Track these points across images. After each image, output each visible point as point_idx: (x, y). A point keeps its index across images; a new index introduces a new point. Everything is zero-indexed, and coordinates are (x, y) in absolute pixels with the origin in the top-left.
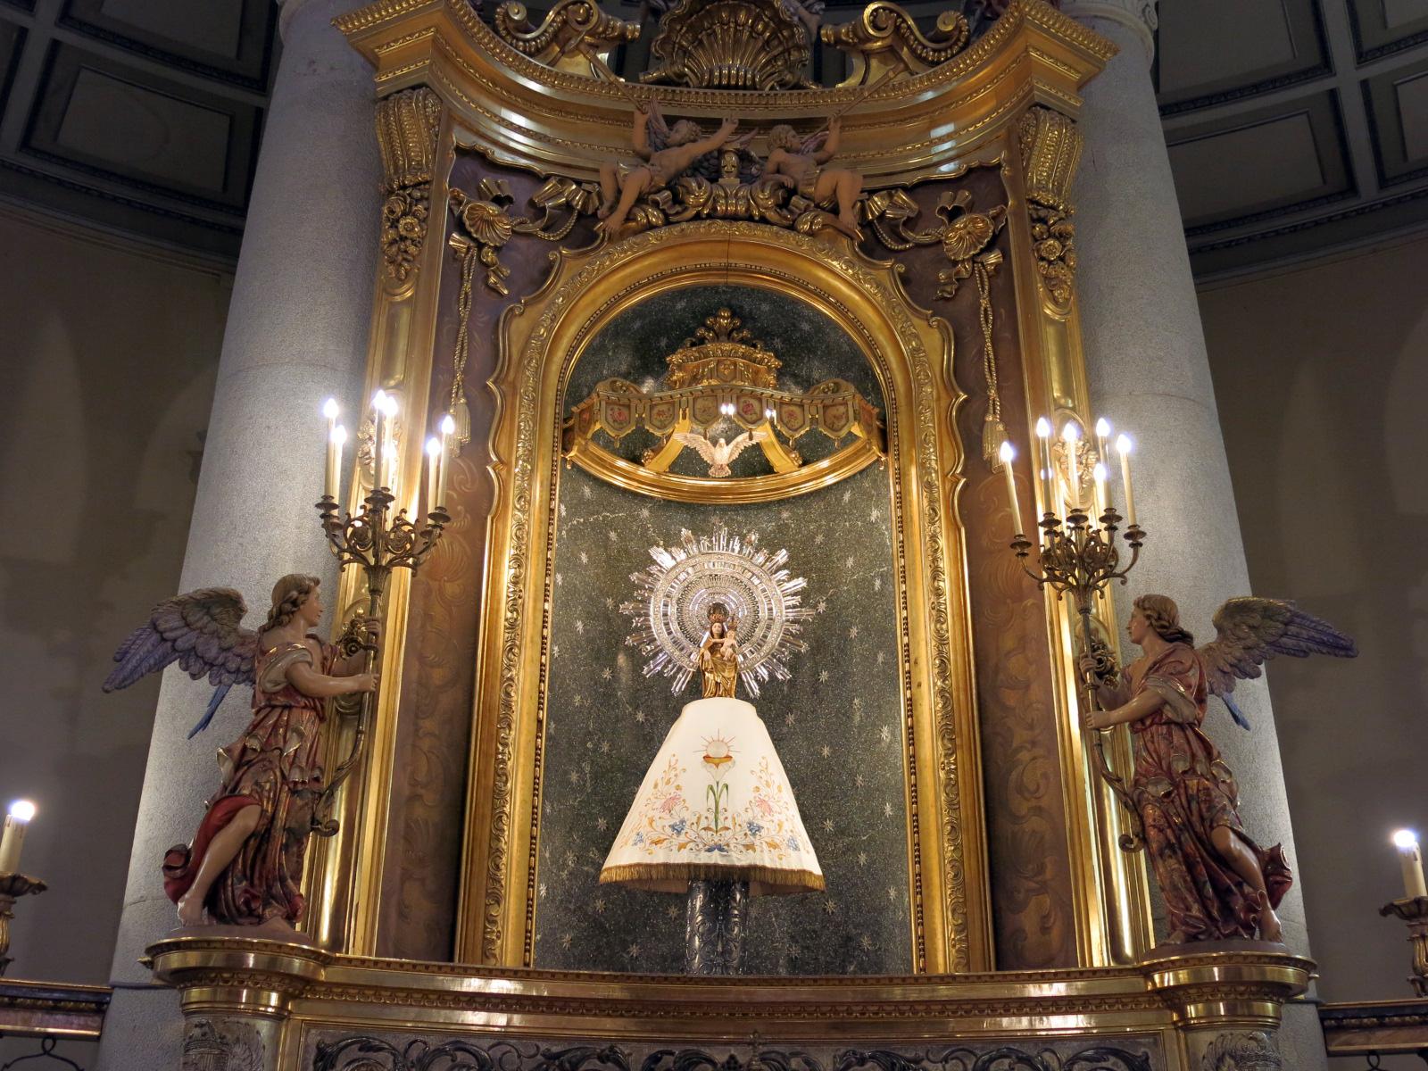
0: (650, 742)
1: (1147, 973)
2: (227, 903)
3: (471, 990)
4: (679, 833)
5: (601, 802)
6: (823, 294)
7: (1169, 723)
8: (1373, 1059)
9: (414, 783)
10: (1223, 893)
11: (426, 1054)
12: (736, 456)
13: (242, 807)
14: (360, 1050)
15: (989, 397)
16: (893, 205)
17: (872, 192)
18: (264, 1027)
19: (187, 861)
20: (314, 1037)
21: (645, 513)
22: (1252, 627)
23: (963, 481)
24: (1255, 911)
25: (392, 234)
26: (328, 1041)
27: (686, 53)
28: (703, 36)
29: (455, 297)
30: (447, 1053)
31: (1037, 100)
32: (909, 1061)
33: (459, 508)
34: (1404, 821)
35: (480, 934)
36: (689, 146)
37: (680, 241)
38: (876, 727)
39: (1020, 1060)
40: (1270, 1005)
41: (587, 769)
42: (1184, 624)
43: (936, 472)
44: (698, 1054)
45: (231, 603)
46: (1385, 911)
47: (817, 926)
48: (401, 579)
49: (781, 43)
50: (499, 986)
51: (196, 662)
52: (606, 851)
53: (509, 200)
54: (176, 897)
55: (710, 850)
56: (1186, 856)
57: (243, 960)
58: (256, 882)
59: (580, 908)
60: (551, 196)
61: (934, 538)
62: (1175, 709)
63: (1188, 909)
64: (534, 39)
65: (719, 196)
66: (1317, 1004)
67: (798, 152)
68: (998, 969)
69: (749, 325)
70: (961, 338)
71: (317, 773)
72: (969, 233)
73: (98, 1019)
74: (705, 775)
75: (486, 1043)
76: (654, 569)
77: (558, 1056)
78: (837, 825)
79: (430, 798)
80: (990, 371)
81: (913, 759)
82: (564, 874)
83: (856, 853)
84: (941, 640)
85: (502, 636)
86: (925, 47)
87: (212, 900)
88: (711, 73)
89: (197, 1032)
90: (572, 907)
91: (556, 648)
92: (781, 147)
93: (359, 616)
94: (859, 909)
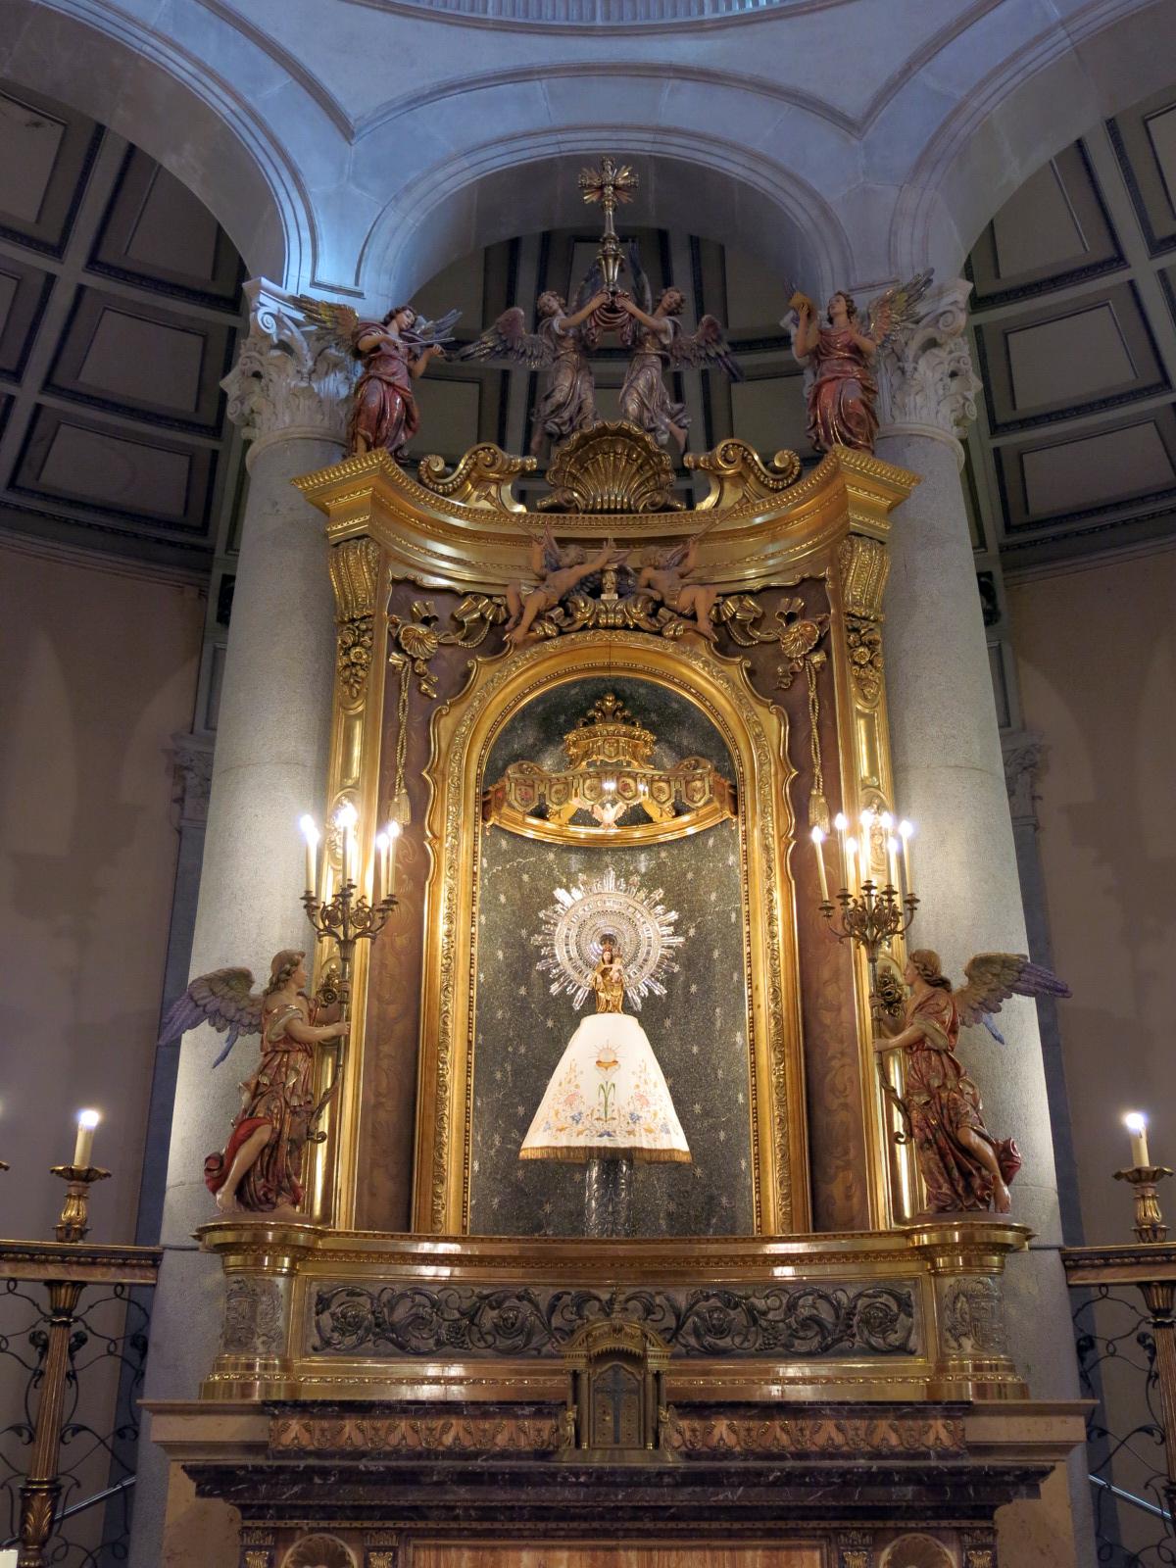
0: (557, 1044)
1: (907, 1235)
2: (251, 1196)
3: (424, 1251)
4: (577, 1122)
5: (520, 1094)
6: (686, 685)
7: (929, 1049)
8: (1104, 1290)
9: (378, 1094)
10: (966, 1175)
11: (393, 1297)
12: (620, 814)
13: (258, 1126)
14: (348, 1295)
15: (814, 775)
16: (742, 609)
17: (726, 596)
18: (281, 1281)
19: (222, 1164)
20: (315, 1287)
21: (551, 856)
22: (994, 975)
23: (794, 842)
24: (989, 1189)
25: (345, 661)
26: (325, 1290)
27: (575, 478)
28: (588, 465)
29: (395, 706)
30: (408, 1296)
31: (852, 530)
32: (740, 1297)
33: (404, 876)
34: (1136, 1105)
35: (429, 1206)
36: (577, 568)
37: (571, 647)
38: (732, 1032)
39: (821, 1297)
40: (996, 1258)
41: (509, 1068)
42: (945, 973)
43: (773, 837)
44: (589, 1293)
45: (244, 977)
46: (1118, 1176)
47: (689, 1188)
48: (362, 946)
49: (651, 468)
50: (442, 1248)
51: (219, 1019)
52: (524, 1132)
53: (435, 618)
54: (215, 1189)
55: (601, 1136)
56: (939, 1148)
57: (265, 1236)
58: (270, 1178)
59: (505, 1177)
60: (469, 612)
61: (770, 891)
62: (932, 1040)
63: (940, 1188)
64: (451, 482)
65: (601, 610)
66: (1060, 1249)
67: (664, 568)
68: (815, 1230)
69: (631, 703)
70: (795, 723)
71: (309, 1098)
72: (801, 635)
73: (153, 1271)
74: (596, 1077)
75: (436, 1288)
76: (558, 907)
77: (487, 1297)
78: (703, 1109)
79: (390, 1104)
80: (816, 753)
81: (754, 1063)
82: (492, 1152)
83: (717, 1131)
84: (775, 974)
85: (439, 978)
86: (766, 476)
87: (240, 1191)
88: (595, 499)
89: (235, 1286)
90: (499, 1177)
91: (482, 976)
92: (650, 566)
93: (333, 970)
94: (719, 1176)
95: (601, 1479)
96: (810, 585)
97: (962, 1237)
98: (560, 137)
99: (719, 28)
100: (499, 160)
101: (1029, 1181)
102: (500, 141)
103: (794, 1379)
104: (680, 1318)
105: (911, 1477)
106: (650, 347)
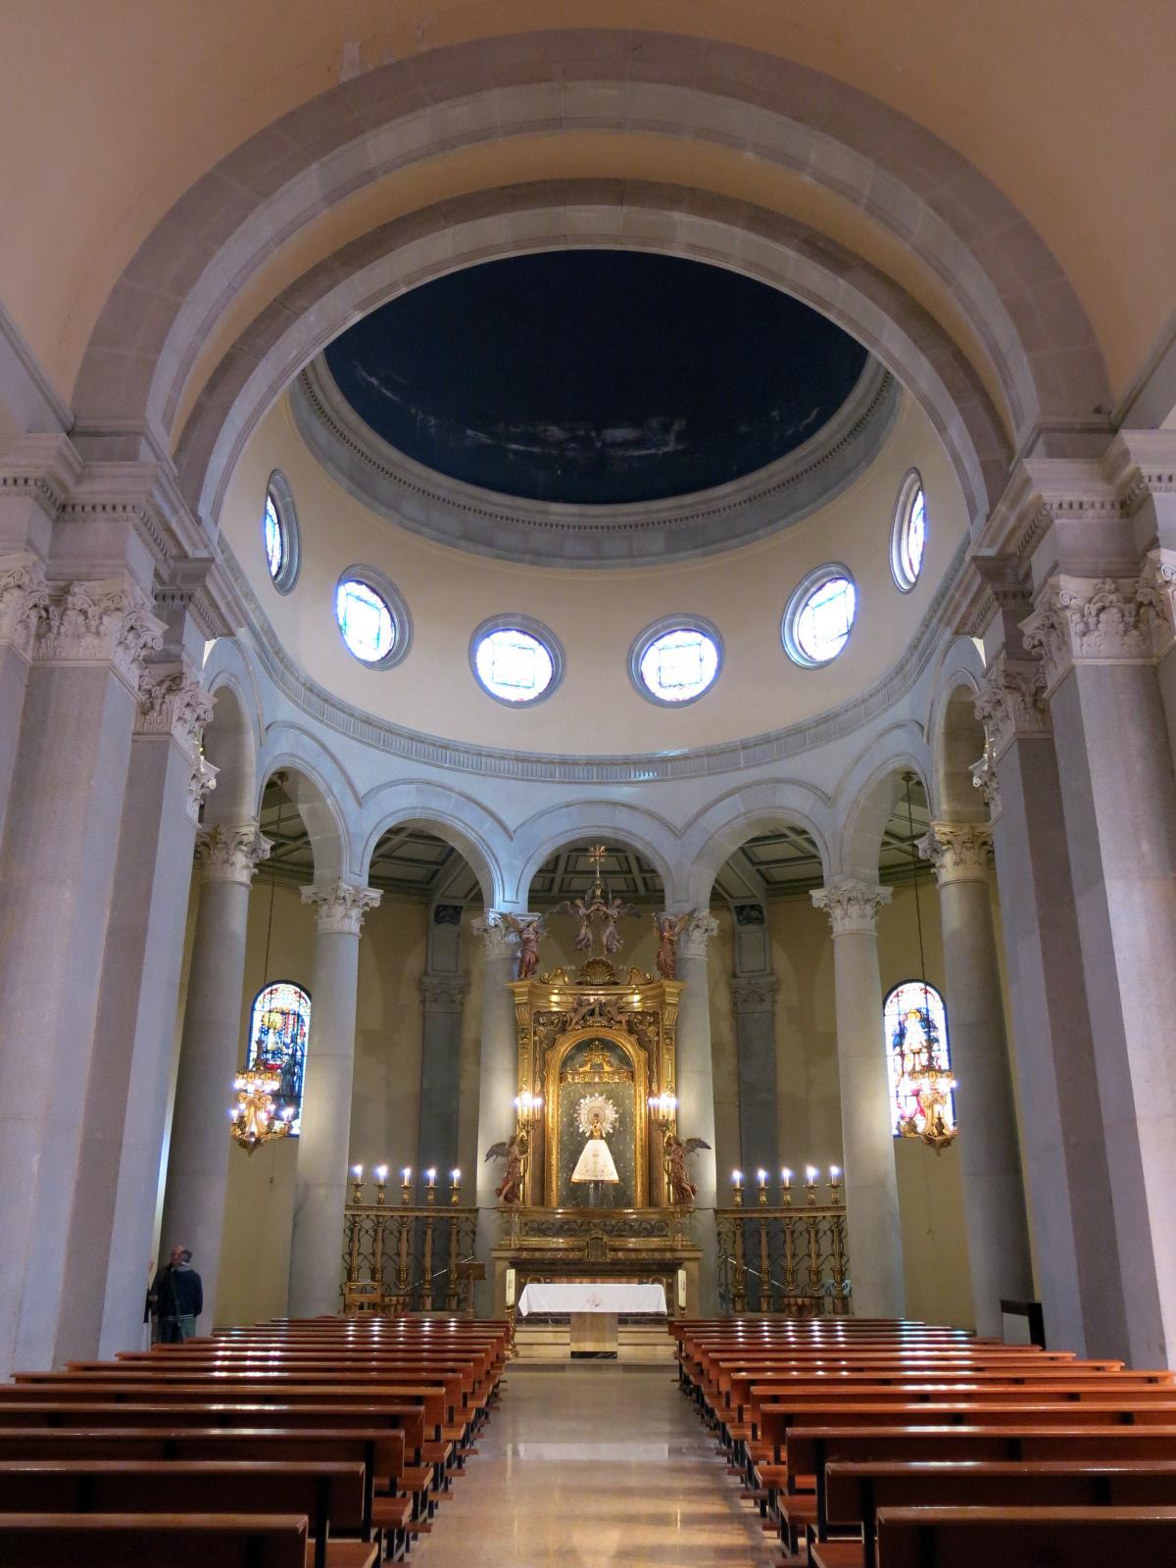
42: (680, 1141)
87: (505, 1197)
95: (593, 1264)
96: (655, 1014)
100: (561, 841)
103: (632, 1242)
104: (613, 1227)
105: (655, 1264)
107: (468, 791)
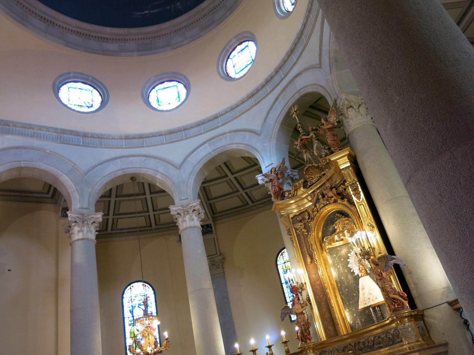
77: (345, 347)
97: (396, 317)
98: (287, 106)
99: (298, 60)
101: (422, 294)
102: (279, 115)
106: (313, 140)
107: (235, 128)
